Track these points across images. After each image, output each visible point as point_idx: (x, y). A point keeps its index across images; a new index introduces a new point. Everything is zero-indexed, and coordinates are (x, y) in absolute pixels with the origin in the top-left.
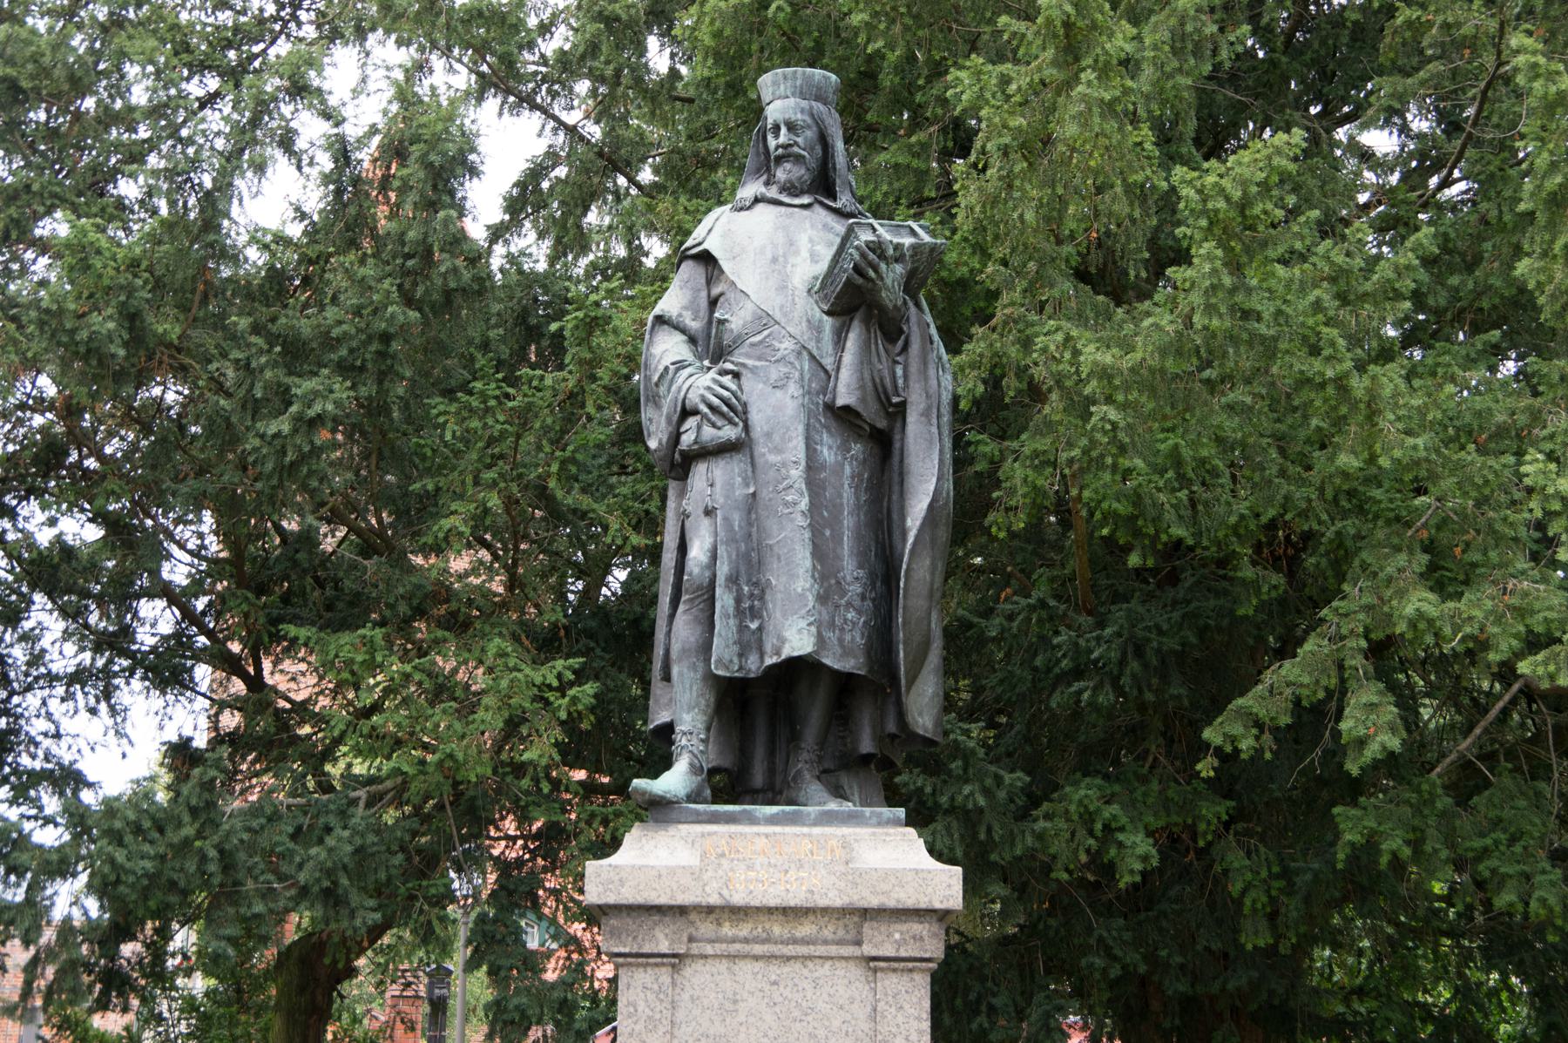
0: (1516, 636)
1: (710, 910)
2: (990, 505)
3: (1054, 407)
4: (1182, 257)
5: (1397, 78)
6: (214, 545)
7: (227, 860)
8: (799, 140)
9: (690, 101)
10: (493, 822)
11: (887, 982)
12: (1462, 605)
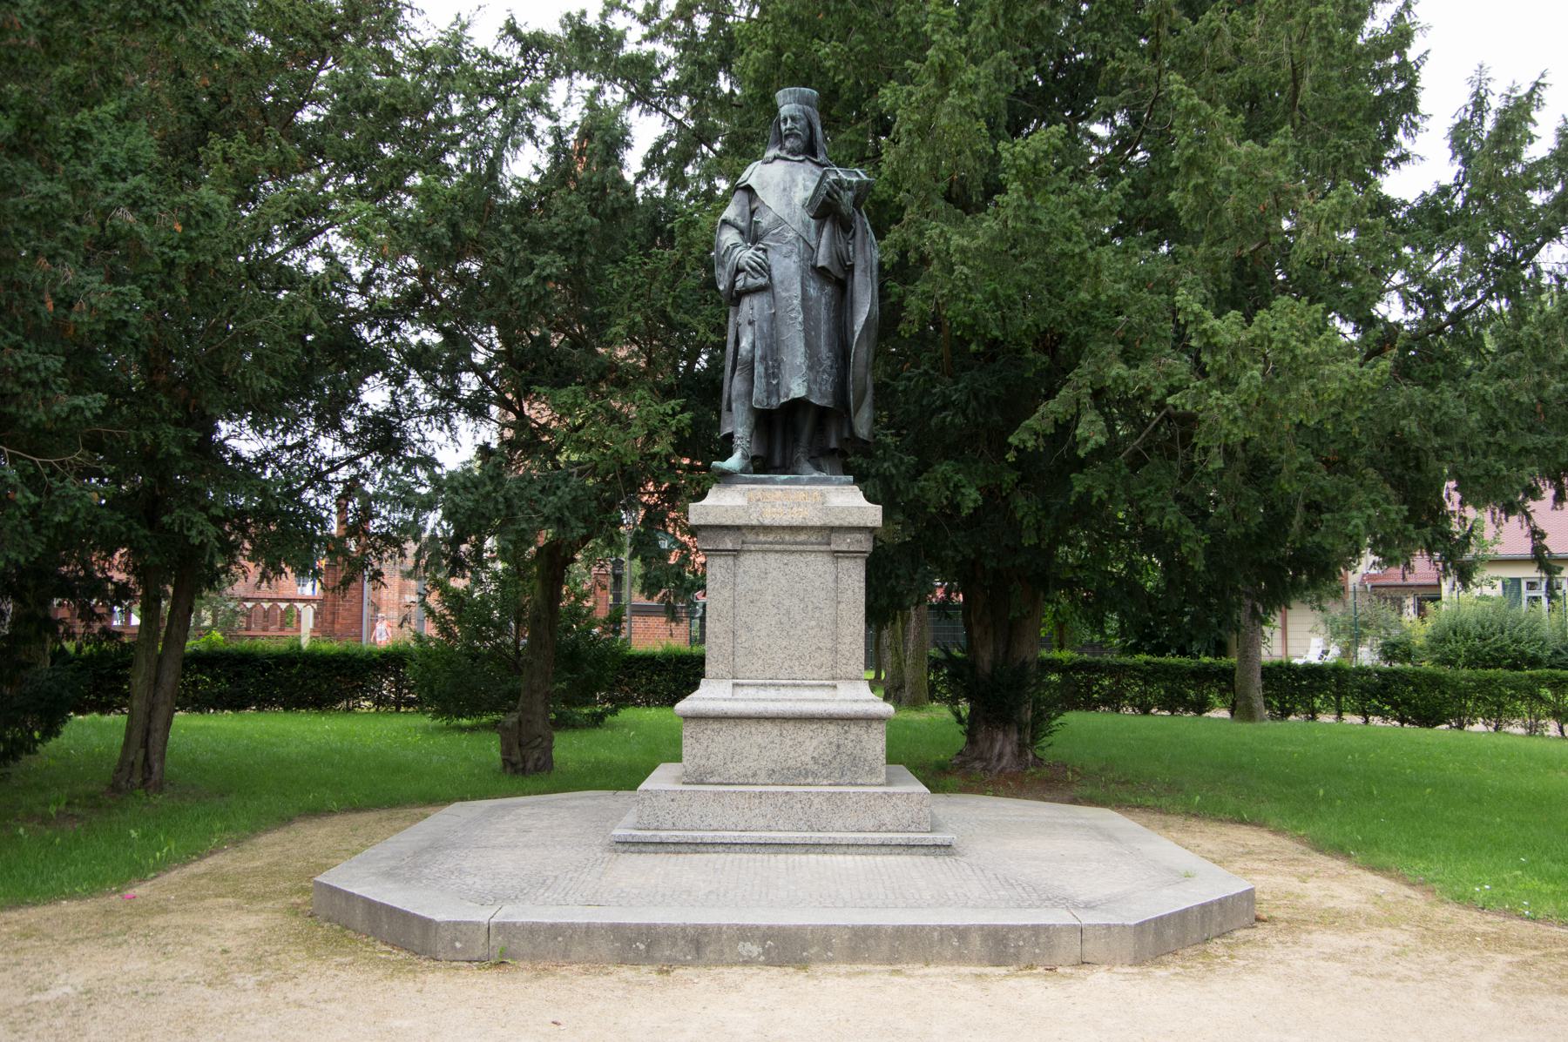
0: (1165, 387)
1: (752, 528)
2: (899, 320)
3: (935, 268)
4: (1001, 188)
5: (1109, 98)
6: (498, 345)
7: (508, 502)
9: (741, 106)
10: (643, 486)
12: (1139, 371)
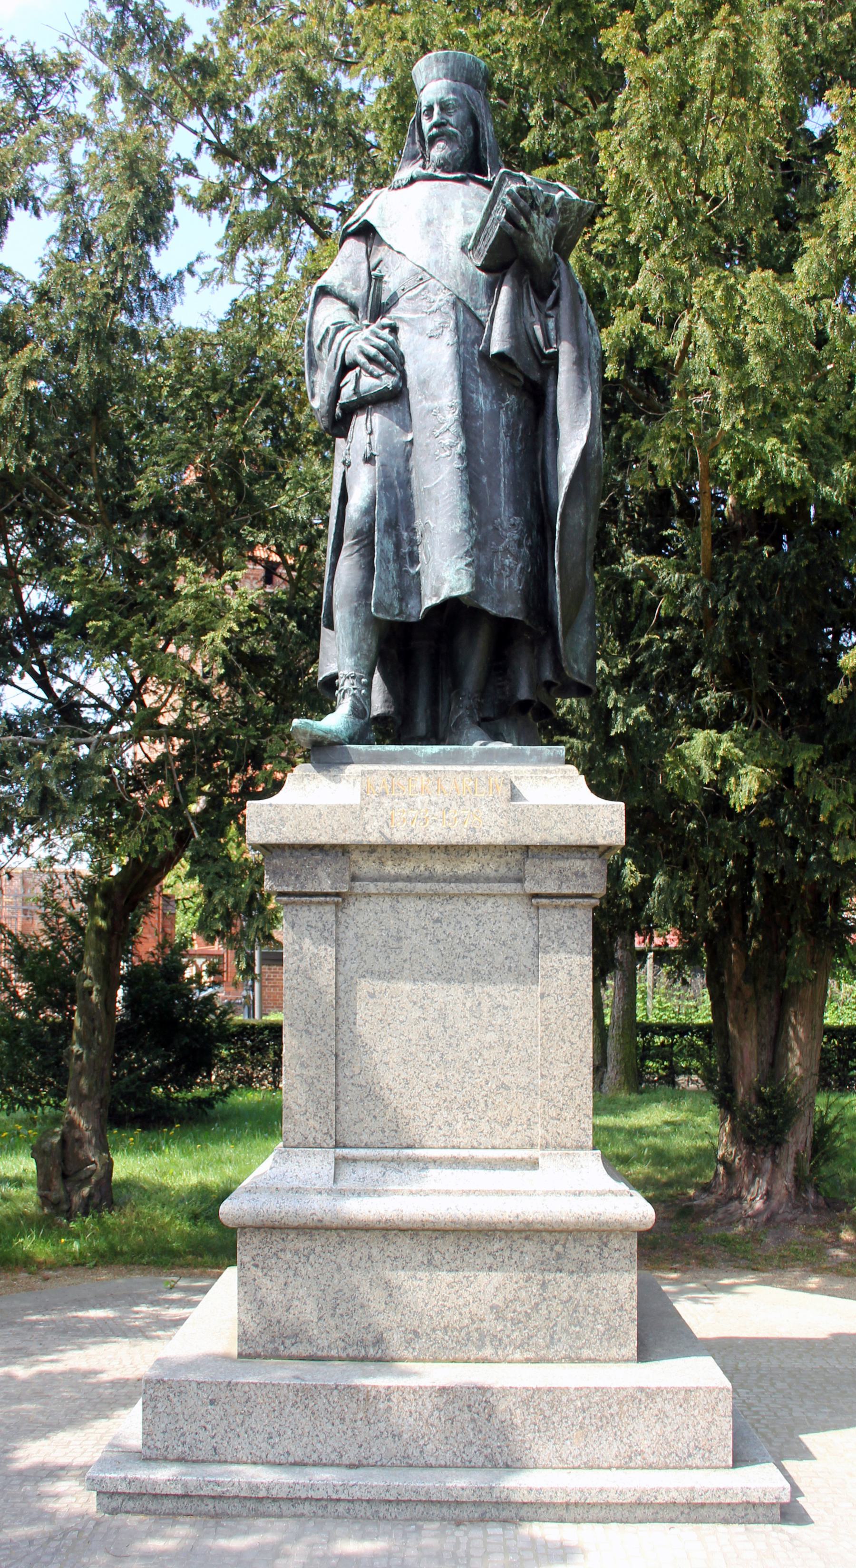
1: (372, 849)
8: (452, 120)
11: (549, 919)
